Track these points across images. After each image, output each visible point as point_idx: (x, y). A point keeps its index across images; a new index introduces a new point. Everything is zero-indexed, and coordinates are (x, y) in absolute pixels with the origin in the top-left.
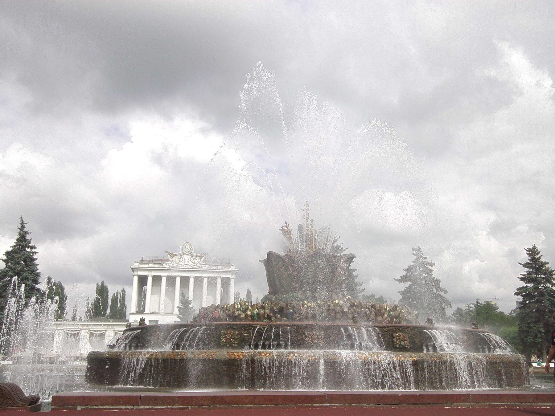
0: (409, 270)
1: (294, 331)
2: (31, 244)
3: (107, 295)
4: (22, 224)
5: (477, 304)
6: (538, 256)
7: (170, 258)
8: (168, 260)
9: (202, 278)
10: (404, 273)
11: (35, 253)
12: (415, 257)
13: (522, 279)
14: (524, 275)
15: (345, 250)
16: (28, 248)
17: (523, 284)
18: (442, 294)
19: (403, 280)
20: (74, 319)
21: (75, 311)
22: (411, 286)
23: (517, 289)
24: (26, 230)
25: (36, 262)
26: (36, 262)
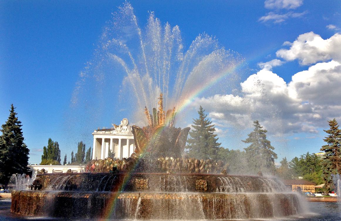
0: (251, 135)
1: (31, 204)
2: (18, 121)
3: (84, 149)
4: (13, 108)
5: (104, 216)
6: (336, 126)
7: (115, 128)
8: (114, 129)
9: (117, 140)
10: (248, 137)
11: (20, 126)
12: (255, 127)
13: (326, 141)
14: (327, 138)
15: (210, 123)
16: (16, 123)
17: (326, 144)
18: (272, 150)
19: (248, 141)
20: (65, 163)
21: (325, 137)
22: (252, 145)
23: (322, 147)
24: (14, 112)
25: (21, 131)
26: (21, 131)
